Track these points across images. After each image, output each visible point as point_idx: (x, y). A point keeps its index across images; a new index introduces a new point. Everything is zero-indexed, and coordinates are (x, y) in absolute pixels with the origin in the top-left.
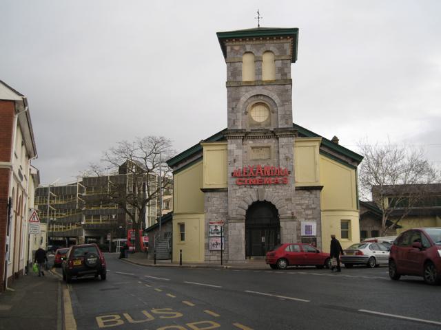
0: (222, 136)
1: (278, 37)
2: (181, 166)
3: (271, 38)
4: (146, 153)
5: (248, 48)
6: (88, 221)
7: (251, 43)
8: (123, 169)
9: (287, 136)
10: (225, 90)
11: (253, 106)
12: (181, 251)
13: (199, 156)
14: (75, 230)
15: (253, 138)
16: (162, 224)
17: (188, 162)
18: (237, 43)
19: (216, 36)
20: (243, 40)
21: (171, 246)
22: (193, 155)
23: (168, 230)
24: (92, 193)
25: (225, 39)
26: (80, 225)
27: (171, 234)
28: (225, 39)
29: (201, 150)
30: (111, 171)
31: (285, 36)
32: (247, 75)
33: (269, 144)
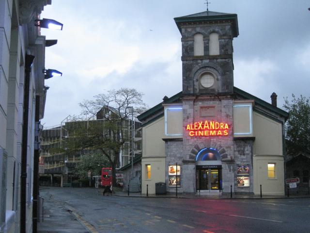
0: (177, 98)
1: (221, 21)
2: (148, 120)
3: (216, 22)
4: (119, 104)
5: (198, 29)
6: (71, 160)
7: (201, 26)
8: (100, 115)
9: (227, 99)
10: (181, 63)
11: (202, 75)
12: (147, 185)
13: (162, 113)
14: (60, 168)
15: (202, 100)
16: (134, 164)
17: (154, 117)
18: (190, 26)
19: (174, 21)
20: (194, 23)
21: (141, 182)
22: (155, 113)
23: (139, 169)
24: (73, 135)
25: (181, 22)
26: (64, 163)
27: (140, 172)
28: (181, 22)
29: (163, 109)
30: (91, 117)
31: (227, 21)
32: (199, 51)
33: (214, 105)
